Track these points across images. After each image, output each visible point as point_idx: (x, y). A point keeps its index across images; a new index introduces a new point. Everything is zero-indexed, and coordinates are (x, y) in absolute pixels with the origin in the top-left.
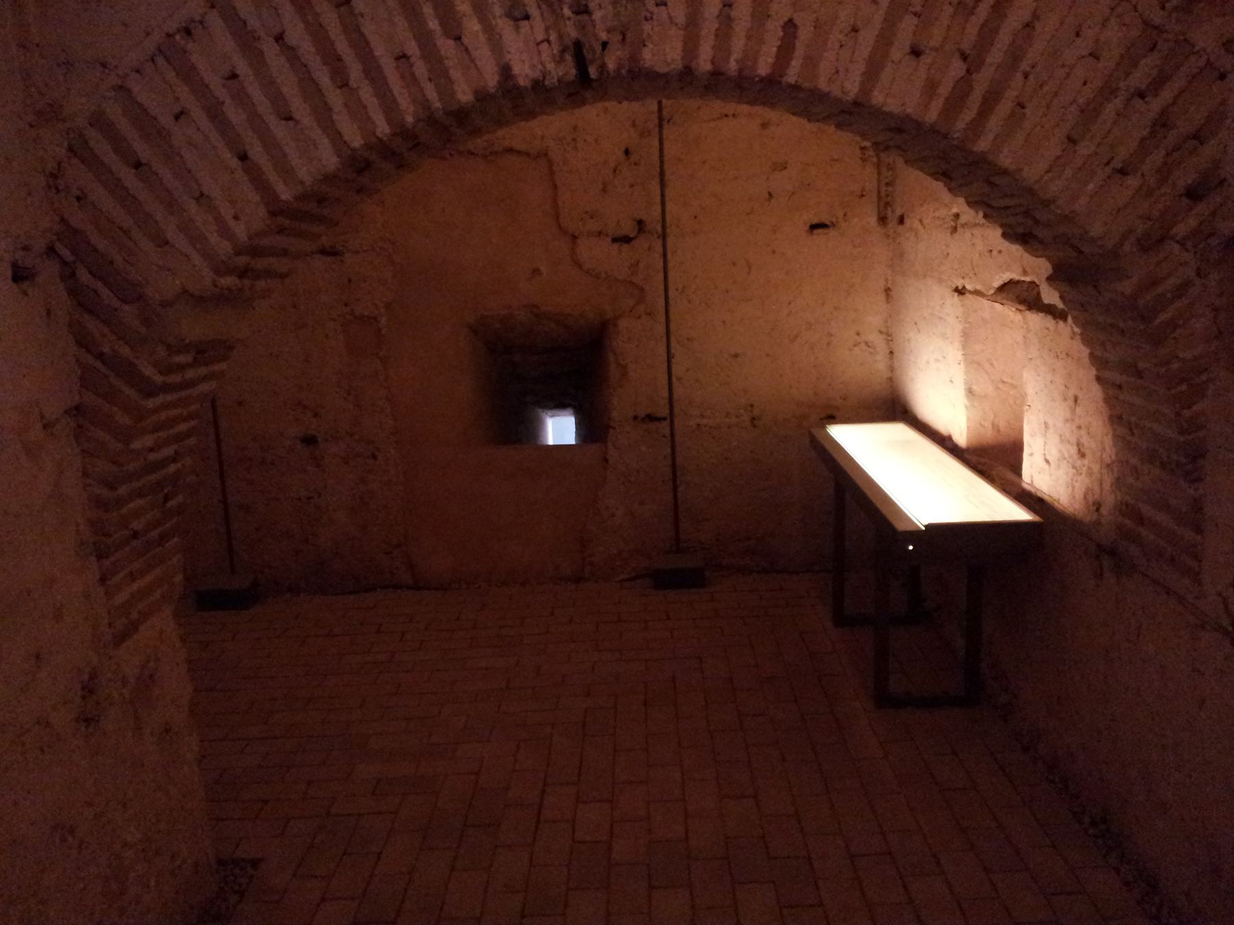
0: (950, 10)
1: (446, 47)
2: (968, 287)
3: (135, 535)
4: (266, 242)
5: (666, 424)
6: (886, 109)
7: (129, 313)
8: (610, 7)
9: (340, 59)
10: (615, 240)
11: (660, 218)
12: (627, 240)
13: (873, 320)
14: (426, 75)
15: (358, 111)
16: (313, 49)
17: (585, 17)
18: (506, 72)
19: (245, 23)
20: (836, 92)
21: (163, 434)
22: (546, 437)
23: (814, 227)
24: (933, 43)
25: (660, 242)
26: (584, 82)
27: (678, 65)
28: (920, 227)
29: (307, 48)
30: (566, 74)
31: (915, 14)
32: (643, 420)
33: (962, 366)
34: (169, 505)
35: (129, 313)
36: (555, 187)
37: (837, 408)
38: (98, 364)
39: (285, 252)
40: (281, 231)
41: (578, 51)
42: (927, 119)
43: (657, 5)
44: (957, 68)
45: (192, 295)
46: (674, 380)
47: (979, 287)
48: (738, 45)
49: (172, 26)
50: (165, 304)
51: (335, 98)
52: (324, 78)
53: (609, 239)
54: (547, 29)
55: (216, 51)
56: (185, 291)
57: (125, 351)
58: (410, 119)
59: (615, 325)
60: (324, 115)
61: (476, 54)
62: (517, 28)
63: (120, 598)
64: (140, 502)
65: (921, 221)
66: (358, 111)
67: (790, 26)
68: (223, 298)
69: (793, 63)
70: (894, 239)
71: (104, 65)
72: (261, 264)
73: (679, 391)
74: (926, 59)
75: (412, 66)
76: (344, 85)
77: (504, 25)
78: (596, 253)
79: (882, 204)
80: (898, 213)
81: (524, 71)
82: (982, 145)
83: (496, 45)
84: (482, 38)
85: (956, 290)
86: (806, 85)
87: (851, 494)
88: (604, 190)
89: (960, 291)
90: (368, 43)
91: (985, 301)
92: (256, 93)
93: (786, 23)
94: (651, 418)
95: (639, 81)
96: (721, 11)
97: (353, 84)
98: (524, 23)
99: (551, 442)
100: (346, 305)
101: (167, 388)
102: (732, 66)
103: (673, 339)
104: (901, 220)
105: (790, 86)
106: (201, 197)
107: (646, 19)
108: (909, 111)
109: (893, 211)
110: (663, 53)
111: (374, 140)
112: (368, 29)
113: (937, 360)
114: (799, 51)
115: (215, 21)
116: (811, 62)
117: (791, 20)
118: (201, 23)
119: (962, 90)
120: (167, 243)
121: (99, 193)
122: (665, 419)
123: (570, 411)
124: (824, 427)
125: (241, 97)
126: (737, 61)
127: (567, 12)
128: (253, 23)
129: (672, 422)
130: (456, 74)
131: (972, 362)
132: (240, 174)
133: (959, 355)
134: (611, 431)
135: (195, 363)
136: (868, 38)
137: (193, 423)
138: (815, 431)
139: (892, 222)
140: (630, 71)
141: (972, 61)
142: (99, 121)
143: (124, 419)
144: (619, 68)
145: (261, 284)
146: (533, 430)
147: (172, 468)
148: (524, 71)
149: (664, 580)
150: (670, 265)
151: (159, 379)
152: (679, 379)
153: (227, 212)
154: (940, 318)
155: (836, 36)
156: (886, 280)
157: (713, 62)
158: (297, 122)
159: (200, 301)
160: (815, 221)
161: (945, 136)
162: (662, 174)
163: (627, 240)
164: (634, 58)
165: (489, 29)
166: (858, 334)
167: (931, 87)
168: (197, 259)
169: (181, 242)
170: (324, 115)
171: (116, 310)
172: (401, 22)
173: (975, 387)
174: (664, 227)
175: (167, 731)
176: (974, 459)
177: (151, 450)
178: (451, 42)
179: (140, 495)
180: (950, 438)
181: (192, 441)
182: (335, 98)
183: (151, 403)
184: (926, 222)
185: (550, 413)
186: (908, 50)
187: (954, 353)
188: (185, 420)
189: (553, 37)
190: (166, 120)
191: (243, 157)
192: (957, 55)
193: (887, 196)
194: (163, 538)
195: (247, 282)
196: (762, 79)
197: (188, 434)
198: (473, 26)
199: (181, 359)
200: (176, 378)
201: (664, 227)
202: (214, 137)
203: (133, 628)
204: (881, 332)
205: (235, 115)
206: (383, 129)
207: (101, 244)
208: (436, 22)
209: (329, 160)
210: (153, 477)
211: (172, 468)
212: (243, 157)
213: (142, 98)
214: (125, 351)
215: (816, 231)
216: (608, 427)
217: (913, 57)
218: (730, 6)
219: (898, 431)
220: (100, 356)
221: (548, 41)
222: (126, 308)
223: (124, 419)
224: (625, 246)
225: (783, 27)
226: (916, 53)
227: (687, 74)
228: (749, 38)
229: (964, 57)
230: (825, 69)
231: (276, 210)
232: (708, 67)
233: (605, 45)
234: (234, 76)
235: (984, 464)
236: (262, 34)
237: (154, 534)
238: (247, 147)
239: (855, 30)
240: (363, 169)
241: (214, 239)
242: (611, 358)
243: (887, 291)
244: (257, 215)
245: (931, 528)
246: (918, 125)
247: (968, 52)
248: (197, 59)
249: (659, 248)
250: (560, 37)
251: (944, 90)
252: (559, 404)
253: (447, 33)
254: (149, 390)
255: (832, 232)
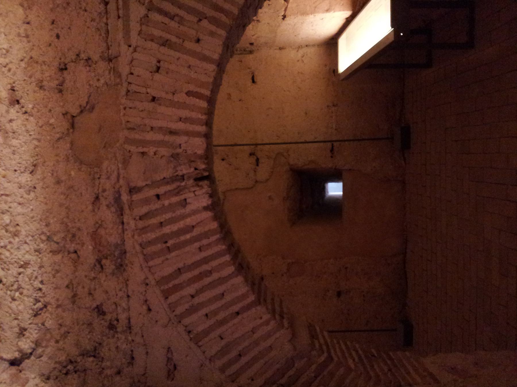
0: (181, 27)
1: (196, 232)
2: (283, 14)
3: (390, 370)
4: (270, 307)
5: (335, 144)
6: (221, 52)
7: (298, 365)
8: (182, 166)
9: (201, 273)
10: (258, 165)
11: (248, 146)
12: (257, 160)
13: (293, 54)
14: (207, 240)
15: (222, 266)
16: (197, 283)
17: (185, 177)
18: (206, 208)
19: (186, 310)
20: (213, 74)
21: (347, 355)
22: (339, 195)
23: (253, 81)
24: (195, 34)
25: (259, 146)
26: (206, 178)
27: (203, 139)
28: (256, 35)
29: (197, 286)
30: (207, 185)
31: (183, 41)
32: (332, 154)
33: (316, 15)
34: (376, 355)
35: (298, 365)
36: (236, 189)
37: (330, 69)
38: (319, 379)
39: (273, 299)
40: (265, 300)
41: (199, 179)
42: (225, 35)
43: (180, 148)
44: (205, 23)
45: (292, 338)
46: (316, 140)
47: (283, 9)
48: (194, 115)
49: (186, 337)
50: (295, 349)
51: (215, 276)
52: (207, 280)
53: (257, 167)
54: (190, 192)
55: (197, 321)
56: (290, 341)
57: (314, 367)
58: (224, 247)
59: (292, 165)
60: (222, 281)
61: (199, 220)
62: (189, 203)
63: (419, 380)
64: (376, 367)
65: (253, 36)
66: (222, 266)
67: (189, 93)
68: (292, 325)
69: (202, 92)
70: (260, 47)
71: (202, 366)
72: (278, 308)
73: (321, 138)
74: (201, 37)
75: (203, 245)
76: (210, 272)
77: (189, 209)
78: (263, 172)
79: (245, 52)
80: (248, 45)
81: (205, 201)
82: (236, 11)
83: (194, 212)
84: (193, 217)
85: (283, 19)
86: (211, 87)
87: (373, 63)
88: (238, 169)
89: (284, 17)
90: (195, 262)
91: (289, 6)
92: (213, 307)
93: (187, 95)
94: (332, 150)
95: (208, 156)
96: (183, 122)
97: (210, 269)
98: (188, 201)
99: (341, 193)
100: (283, 275)
101: (329, 352)
102: (204, 117)
103: (298, 141)
104: (252, 44)
105: (211, 94)
106: (253, 331)
107: (186, 152)
108: (221, 43)
109: (248, 48)
110: (198, 145)
111: (232, 262)
112: (189, 262)
113: (312, 26)
114: (198, 90)
115: (187, 321)
116: (202, 85)
117: (186, 94)
118: (186, 327)
119: (214, 21)
120: (270, 346)
121: (250, 372)
122: (333, 144)
123: (326, 185)
124: (339, 75)
125: (215, 313)
126: (202, 115)
127: (183, 184)
128: (187, 306)
129: (333, 141)
130: (206, 229)
131: (314, 10)
132: (245, 315)
133: (311, 16)
134: (337, 167)
135: (317, 339)
136: (193, 61)
137: (341, 342)
138: (342, 78)
139: (253, 48)
140: (206, 159)
141: (201, 17)
142: (222, 370)
143: (342, 371)
144: (204, 163)
145: (285, 310)
146: (335, 200)
147: (360, 352)
148: (205, 201)
149: (406, 144)
150: (268, 142)
151: (325, 355)
152: (316, 138)
153: (259, 322)
154: (295, 25)
155: (193, 75)
156: (276, 49)
157: (202, 125)
158: (225, 291)
159: (294, 335)
160: (251, 81)
161: (231, 27)
162: (231, 145)
163: (257, 160)
164: (200, 157)
165: (189, 215)
166: (298, 61)
167: (212, 34)
168: (278, 335)
169: (269, 342)
170: (222, 281)
171: (297, 369)
172: (187, 249)
173: (326, 8)
174: (252, 145)
175: (477, 364)
176: (358, 7)
177: (354, 360)
178: (195, 229)
179: (372, 366)
180: (347, 19)
181: (348, 343)
182: (215, 276)
183: (336, 359)
184: (253, 33)
185: (327, 193)
186: (197, 44)
187: (311, 18)
188: (340, 345)
189: (193, 189)
190: (223, 343)
191: (238, 313)
192: (199, 23)
193: (241, 50)
194: (391, 359)
195: (285, 316)
196: (209, 105)
197: (346, 345)
198: (189, 221)
199: (317, 345)
200: (324, 347)
201: (252, 145)
202: (230, 324)
203: (431, 375)
204: (298, 51)
205: (221, 315)
206: (227, 258)
207: (270, 373)
208: (187, 235)
209: (239, 280)
210: (365, 361)
211: (360, 352)
212: (238, 313)
213: (213, 352)
214: (314, 367)
215: (255, 80)
216: (335, 169)
217: (200, 42)
218: (181, 118)
219: (342, 41)
220: (316, 377)
221: (194, 192)
222: (296, 365)
223: (342, 371)
224: (260, 160)
225: (189, 96)
226: (198, 41)
227: (208, 136)
228: (193, 111)
229: (200, 20)
230: (204, 78)
231: (258, 302)
232: (204, 127)
233: (196, 169)
234: (207, 315)
235: (360, 3)
236: (190, 304)
237: (389, 362)
238: (234, 312)
239: (189, 67)
240: (242, 268)
241: (269, 328)
242: (306, 167)
243: (280, 49)
244: (260, 309)
245: (393, 26)
246: (227, 38)
247: (198, 19)
248: (200, 329)
249: (261, 147)
250: (193, 186)
251: (213, 28)
252: (323, 190)
253: (191, 231)
254: (330, 358)
255: (256, 73)
